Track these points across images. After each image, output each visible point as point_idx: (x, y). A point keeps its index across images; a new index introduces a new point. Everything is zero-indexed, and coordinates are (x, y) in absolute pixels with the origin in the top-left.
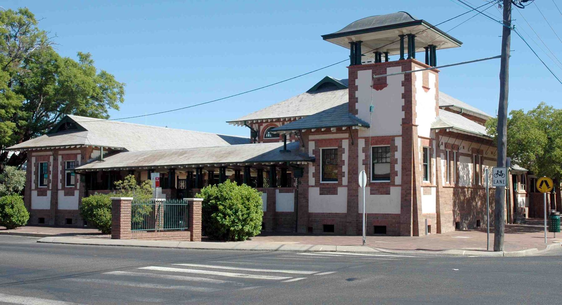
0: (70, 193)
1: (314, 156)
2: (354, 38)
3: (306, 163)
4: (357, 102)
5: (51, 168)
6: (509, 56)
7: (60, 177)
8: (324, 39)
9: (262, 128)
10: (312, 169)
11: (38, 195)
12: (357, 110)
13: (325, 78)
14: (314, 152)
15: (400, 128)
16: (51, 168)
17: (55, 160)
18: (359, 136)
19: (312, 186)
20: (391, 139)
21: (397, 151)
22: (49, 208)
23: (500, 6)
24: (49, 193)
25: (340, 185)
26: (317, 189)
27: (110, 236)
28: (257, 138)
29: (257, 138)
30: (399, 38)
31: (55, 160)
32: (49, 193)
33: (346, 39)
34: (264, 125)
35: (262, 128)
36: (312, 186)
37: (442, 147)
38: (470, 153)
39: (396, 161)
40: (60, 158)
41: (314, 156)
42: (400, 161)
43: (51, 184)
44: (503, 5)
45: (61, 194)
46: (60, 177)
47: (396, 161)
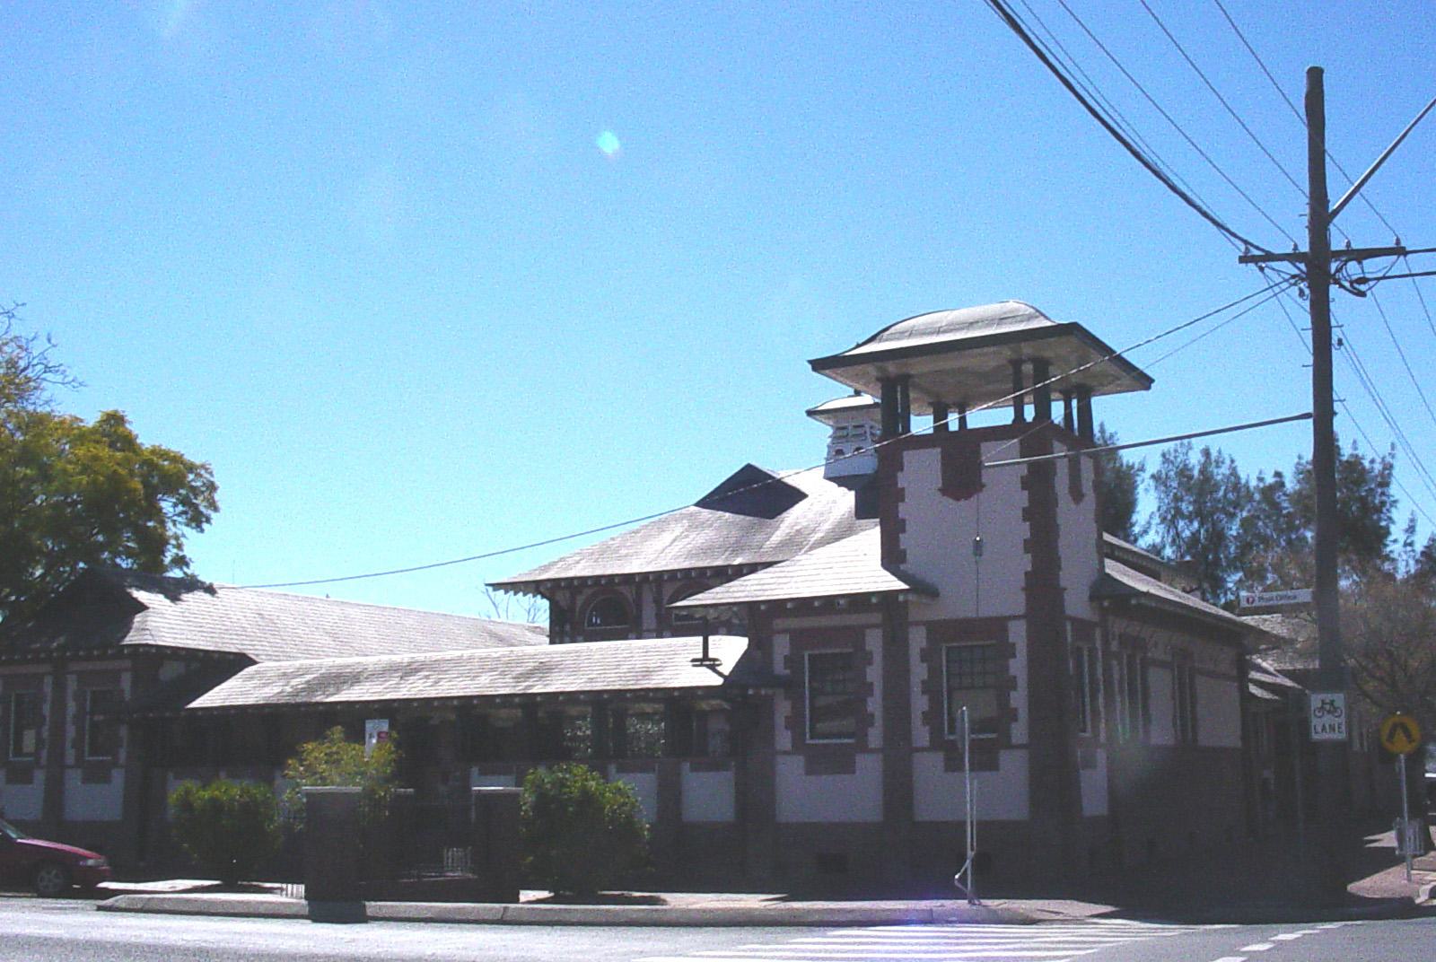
0: (96, 775)
1: (788, 671)
2: (892, 368)
3: (770, 692)
4: (904, 531)
5: (47, 709)
6: (113, 428)
7: (71, 732)
8: (814, 369)
9: (580, 600)
10: (783, 709)
11: (84, 781)
12: (904, 552)
13: (742, 470)
14: (789, 661)
15: (1022, 598)
16: (47, 709)
17: (60, 686)
18: (910, 619)
19: (786, 753)
20: (997, 626)
21: (1014, 656)
22: (919, 818)
23: (1301, 293)
24: (40, 776)
25: (864, 748)
26: (798, 762)
27: (292, 894)
28: (568, 627)
29: (568, 627)
30: (1010, 370)
31: (60, 686)
32: (40, 776)
33: (871, 370)
34: (588, 592)
35: (580, 600)
36: (786, 753)
37: (1114, 646)
38: (1169, 658)
39: (1012, 683)
40: (72, 684)
41: (788, 671)
42: (1022, 682)
43: (44, 753)
44: (1307, 291)
45: (74, 779)
46: (71, 732)
47: (1012, 683)
